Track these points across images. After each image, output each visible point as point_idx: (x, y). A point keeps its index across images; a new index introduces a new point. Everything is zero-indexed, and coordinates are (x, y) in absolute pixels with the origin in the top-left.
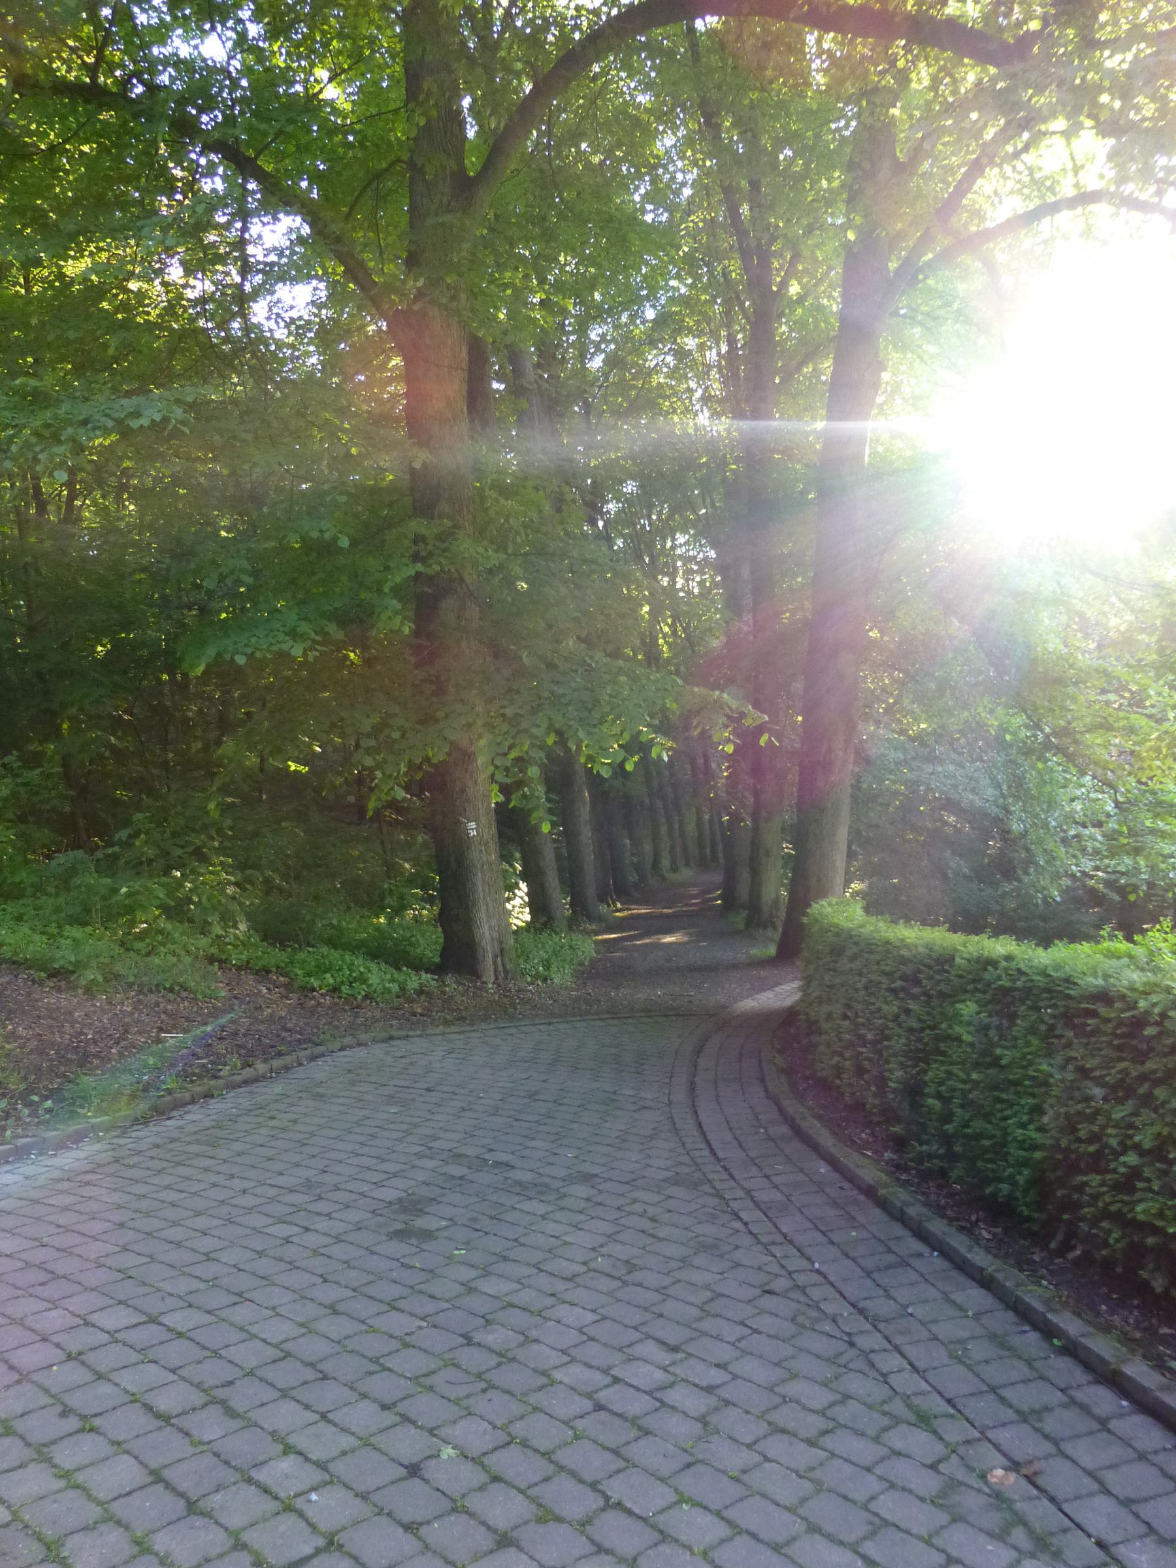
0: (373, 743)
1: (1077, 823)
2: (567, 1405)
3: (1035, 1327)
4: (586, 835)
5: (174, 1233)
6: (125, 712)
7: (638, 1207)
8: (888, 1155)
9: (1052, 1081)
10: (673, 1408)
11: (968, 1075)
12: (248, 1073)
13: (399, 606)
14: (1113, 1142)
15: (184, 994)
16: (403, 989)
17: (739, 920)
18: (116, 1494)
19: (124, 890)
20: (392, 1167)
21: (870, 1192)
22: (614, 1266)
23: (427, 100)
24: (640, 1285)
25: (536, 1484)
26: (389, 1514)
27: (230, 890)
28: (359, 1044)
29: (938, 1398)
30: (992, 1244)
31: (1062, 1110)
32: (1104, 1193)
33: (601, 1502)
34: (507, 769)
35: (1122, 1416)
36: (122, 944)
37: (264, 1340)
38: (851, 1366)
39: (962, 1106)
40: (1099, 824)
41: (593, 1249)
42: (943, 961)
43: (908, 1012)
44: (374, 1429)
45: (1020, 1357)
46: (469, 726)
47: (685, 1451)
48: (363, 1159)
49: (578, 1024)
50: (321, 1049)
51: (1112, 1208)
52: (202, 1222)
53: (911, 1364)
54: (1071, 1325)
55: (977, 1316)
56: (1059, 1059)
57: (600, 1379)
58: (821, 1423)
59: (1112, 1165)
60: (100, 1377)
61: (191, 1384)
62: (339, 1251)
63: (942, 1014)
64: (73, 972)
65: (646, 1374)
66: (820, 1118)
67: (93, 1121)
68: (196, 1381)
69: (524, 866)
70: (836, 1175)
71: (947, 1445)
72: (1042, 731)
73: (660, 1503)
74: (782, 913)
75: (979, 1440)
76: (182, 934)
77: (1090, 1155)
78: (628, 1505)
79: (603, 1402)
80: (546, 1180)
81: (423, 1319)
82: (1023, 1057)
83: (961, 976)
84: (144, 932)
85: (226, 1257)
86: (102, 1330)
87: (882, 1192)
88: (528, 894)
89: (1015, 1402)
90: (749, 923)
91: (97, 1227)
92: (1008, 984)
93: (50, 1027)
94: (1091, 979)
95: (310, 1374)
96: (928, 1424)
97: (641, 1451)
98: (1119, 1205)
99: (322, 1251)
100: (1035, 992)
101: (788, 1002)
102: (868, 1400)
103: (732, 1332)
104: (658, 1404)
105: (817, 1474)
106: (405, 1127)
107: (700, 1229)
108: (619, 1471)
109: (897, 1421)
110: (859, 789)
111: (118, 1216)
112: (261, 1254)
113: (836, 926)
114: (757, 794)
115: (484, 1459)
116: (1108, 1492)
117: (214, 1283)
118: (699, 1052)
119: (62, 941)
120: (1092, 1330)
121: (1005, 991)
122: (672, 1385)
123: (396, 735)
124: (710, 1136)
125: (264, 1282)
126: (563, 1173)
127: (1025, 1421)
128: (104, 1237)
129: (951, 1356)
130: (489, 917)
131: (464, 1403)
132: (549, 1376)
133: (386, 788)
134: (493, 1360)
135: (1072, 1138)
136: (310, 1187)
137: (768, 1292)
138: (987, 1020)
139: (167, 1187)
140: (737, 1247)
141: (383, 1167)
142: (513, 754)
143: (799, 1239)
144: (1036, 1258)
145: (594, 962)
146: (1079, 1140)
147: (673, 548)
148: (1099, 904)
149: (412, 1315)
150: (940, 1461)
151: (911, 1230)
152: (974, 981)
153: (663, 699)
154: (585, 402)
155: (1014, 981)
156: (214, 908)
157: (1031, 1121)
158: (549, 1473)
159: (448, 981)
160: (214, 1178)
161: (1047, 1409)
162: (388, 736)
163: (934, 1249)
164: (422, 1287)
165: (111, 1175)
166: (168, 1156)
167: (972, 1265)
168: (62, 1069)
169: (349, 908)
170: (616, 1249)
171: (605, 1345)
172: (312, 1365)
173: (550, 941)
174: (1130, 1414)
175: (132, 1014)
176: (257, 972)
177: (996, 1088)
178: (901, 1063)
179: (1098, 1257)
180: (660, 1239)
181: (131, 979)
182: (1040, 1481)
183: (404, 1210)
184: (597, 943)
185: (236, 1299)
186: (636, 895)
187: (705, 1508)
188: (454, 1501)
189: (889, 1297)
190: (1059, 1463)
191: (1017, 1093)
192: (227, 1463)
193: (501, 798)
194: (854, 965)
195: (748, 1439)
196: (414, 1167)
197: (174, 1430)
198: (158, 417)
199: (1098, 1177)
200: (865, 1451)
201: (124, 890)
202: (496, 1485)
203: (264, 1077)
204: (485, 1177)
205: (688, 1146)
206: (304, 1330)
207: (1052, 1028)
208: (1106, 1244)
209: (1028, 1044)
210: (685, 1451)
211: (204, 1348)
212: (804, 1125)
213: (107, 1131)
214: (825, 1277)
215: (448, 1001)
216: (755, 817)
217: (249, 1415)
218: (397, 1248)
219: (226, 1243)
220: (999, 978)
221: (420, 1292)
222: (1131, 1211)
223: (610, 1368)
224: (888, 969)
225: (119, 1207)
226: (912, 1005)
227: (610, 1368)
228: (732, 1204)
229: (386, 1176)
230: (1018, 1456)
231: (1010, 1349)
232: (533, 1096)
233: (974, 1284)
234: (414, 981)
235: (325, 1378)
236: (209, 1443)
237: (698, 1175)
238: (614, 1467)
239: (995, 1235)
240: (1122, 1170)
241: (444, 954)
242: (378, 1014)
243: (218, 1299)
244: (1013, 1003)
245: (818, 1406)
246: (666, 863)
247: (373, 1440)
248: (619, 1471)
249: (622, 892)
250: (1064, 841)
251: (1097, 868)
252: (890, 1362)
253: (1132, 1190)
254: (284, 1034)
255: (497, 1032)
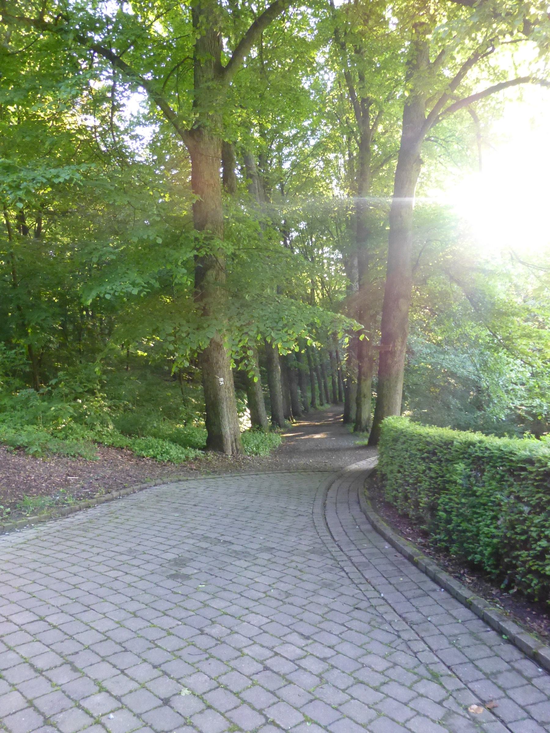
0: (173, 338)
1: (512, 383)
2: (253, 667)
3: (494, 629)
4: (279, 387)
5: (61, 575)
6: (60, 326)
7: (294, 564)
8: (419, 540)
9: (502, 503)
10: (305, 670)
11: (460, 500)
12: (108, 496)
13: (185, 271)
14: (534, 535)
15: (80, 458)
16: (187, 457)
17: (351, 428)
18: (7, 713)
19: (53, 408)
20: (173, 543)
21: (410, 558)
22: (280, 594)
23: (201, 27)
24: (292, 604)
25: (230, 710)
26: (151, 727)
27: (105, 409)
28: (164, 483)
29: (443, 666)
30: (471, 585)
31: (508, 518)
32: (529, 561)
33: (264, 721)
34: (237, 352)
35: (539, 676)
36: (52, 434)
37: (97, 631)
38: (398, 648)
39: (457, 516)
40: (523, 384)
41: (270, 585)
42: (448, 444)
43: (430, 469)
44: (148, 679)
45: (485, 644)
46: (220, 331)
47: (310, 693)
48: (160, 539)
49: (271, 475)
50: (145, 485)
51: (533, 568)
52: (75, 569)
53: (429, 647)
54: (512, 628)
55: (464, 622)
56: (506, 492)
57: (268, 653)
58: (383, 679)
59: (533, 546)
60: (10, 649)
61: (56, 653)
62: (141, 585)
63: (447, 470)
64: (27, 447)
65: (290, 651)
66: (386, 521)
67: (29, 518)
68: (59, 652)
69: (249, 401)
70: (393, 550)
71: (447, 691)
72: (497, 338)
73: (295, 722)
74: (371, 424)
75: (464, 689)
76: (81, 430)
77: (522, 541)
78: (278, 722)
79: (268, 666)
80: (248, 550)
81: (179, 620)
82: (488, 492)
83: (457, 451)
84: (63, 429)
85: (83, 587)
86: (15, 624)
87: (416, 558)
88: (250, 414)
89: (483, 668)
90: (355, 429)
91: (22, 571)
92: (481, 455)
93: (14, 473)
94: (523, 452)
95: (118, 648)
96: (438, 680)
97: (288, 693)
98: (536, 567)
99: (132, 584)
100: (494, 458)
101: (372, 466)
102: (407, 666)
103: (337, 629)
104: (297, 667)
105: (379, 707)
106: (182, 523)
107: (324, 576)
108: (274, 704)
109: (422, 678)
110: (409, 366)
111: (33, 566)
112: (101, 585)
113: (396, 427)
114: (360, 368)
115: (204, 696)
116: (532, 718)
117: (76, 600)
118: (328, 489)
119: (23, 432)
120: (523, 631)
121: (479, 458)
122: (305, 657)
123: (184, 335)
124: (332, 529)
125: (102, 600)
126: (257, 546)
127: (488, 679)
128: (24, 576)
129: (450, 643)
130: (229, 423)
131: (196, 665)
132: (241, 652)
133: (180, 361)
134: (214, 642)
135: (512, 532)
136: (131, 552)
137: (357, 608)
138: (470, 473)
139: (61, 551)
140: (342, 585)
141: (168, 543)
142: (241, 345)
143: (374, 581)
144: (494, 593)
145: (280, 446)
146: (516, 533)
147: (323, 254)
148: (523, 423)
149: (174, 618)
150: (443, 700)
151: (430, 577)
152: (463, 453)
153: (313, 317)
154: (281, 183)
155: (483, 453)
156: (97, 418)
157: (492, 523)
158: (238, 704)
159: (209, 454)
160: (84, 547)
161: (500, 672)
162: (180, 336)
163: (442, 588)
164: (181, 604)
165: (34, 545)
166: (63, 536)
167: (461, 596)
168: (17, 493)
169: (164, 419)
170: (281, 586)
171: (272, 635)
172: (120, 644)
173: (259, 436)
174: (543, 676)
175: (55, 467)
176: (117, 448)
177: (474, 507)
178: (427, 494)
179: (526, 593)
180: (304, 581)
181: (55, 451)
182: (495, 711)
183: (176, 564)
184: (282, 437)
185: (86, 608)
186: (303, 416)
187: (319, 725)
188: (186, 719)
189: (418, 612)
190: (506, 701)
191: (484, 509)
192: (69, 697)
193: (235, 366)
194: (404, 446)
195: (343, 687)
196: (183, 543)
197: (44, 678)
198: (67, 178)
199: (526, 552)
200: (403, 694)
201: (53, 408)
202: (209, 710)
203: (116, 498)
204: (218, 548)
205: (320, 534)
206: (119, 625)
207: (503, 476)
208: (529, 586)
209: (490, 485)
210: (310, 693)
211: (66, 634)
212: (378, 525)
213: (36, 523)
214: (386, 601)
215: (209, 463)
216: (359, 379)
217: (84, 670)
218: (170, 583)
219: (86, 580)
220: (476, 452)
221: (180, 606)
222: (543, 569)
223: (273, 647)
224: (420, 448)
225: (35, 561)
226: (432, 466)
227: (273, 647)
228: (340, 563)
229: (169, 547)
230: (485, 697)
231: (481, 640)
232: (246, 508)
233: (462, 606)
234: (192, 454)
235: (126, 651)
236: (60, 686)
237: (325, 548)
238: (271, 702)
239: (473, 581)
240: (538, 549)
241: (209, 441)
242: (174, 469)
243: (77, 608)
244: (483, 464)
245: (380, 669)
246: (317, 402)
247: (146, 685)
248: (274, 704)
249: (296, 415)
250: (507, 392)
251: (522, 405)
252: (419, 646)
253: (544, 559)
254: (128, 478)
255: (231, 478)
